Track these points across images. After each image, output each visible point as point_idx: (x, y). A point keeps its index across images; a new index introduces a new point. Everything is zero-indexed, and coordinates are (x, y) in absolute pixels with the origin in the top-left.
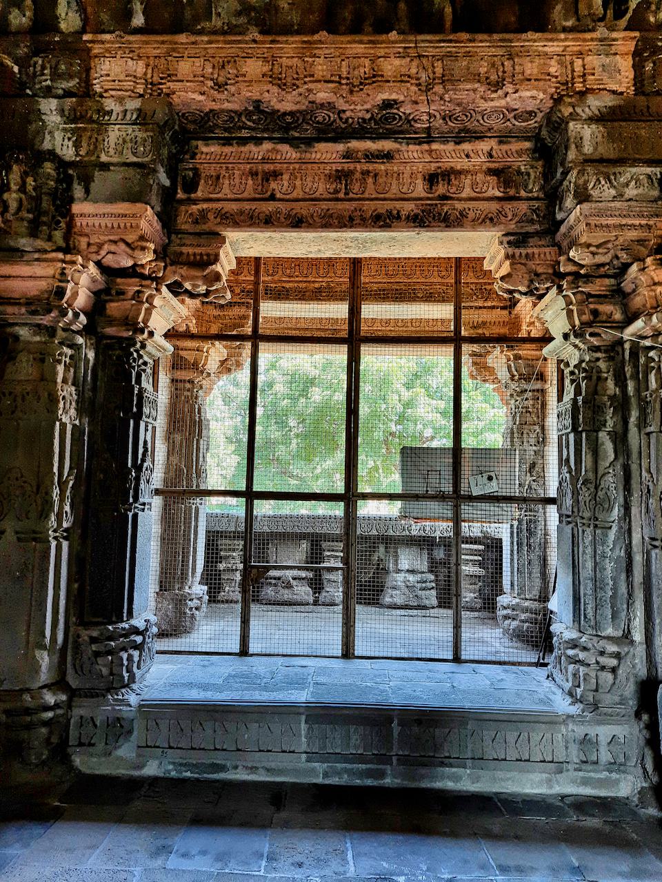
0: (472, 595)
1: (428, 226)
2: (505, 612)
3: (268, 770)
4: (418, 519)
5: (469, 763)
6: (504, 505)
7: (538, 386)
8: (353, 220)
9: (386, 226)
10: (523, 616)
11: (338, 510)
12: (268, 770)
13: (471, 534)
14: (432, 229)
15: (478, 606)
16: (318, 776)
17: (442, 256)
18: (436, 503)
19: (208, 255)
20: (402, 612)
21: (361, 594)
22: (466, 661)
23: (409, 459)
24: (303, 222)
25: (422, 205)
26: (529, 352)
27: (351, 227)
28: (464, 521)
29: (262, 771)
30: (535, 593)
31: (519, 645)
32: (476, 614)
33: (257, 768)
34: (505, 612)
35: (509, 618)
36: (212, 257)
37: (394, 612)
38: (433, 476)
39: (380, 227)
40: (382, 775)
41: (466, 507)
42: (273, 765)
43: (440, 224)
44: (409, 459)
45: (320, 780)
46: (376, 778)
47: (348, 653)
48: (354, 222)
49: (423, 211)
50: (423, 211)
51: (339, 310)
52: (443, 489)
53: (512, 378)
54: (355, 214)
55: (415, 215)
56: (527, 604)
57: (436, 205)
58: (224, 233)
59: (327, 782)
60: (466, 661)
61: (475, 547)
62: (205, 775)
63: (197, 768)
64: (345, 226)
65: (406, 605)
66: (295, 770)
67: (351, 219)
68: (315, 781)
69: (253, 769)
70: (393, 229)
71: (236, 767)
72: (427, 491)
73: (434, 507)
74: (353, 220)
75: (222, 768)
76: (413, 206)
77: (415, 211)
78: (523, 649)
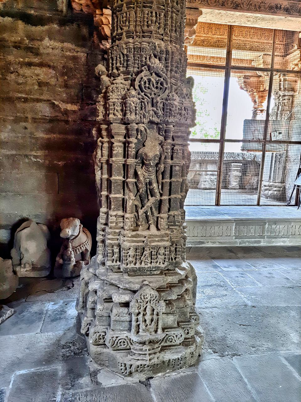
0: (235, 183)
1: (292, 14)
2: (266, 188)
3: (220, 243)
4: (248, 150)
5: (291, 236)
6: (282, 145)
7: (291, 93)
8: (261, 8)
9: (274, 13)
10: (275, 189)
11: (215, 148)
12: (220, 243)
13: (239, 159)
14: (293, 16)
15: (238, 188)
16: (238, 244)
17: (284, 29)
18: (257, 144)
19: (193, 20)
20: (209, 191)
21: (224, 181)
22: (262, 205)
23: (247, 125)
24: (238, 7)
25: (291, 3)
26: (291, 78)
27: (260, 11)
28: (267, 151)
29: (217, 243)
30: (280, 180)
31: (272, 200)
32: (237, 191)
33: (216, 242)
34: (266, 188)
35: (267, 190)
36: (194, 21)
37: (205, 191)
38: (256, 132)
39: (272, 13)
40: (260, 242)
41: (268, 146)
42: (221, 241)
43: (297, 14)
44: (247, 125)
45: (238, 245)
46: (258, 243)
47: (218, 204)
48: (261, 9)
49: (291, 6)
50: (291, 6)
51: (223, 53)
52: (259, 138)
53: (280, 89)
54: (261, 5)
55: (287, 8)
56: (276, 184)
57: (296, 3)
58: (201, 9)
59: (241, 246)
60: (262, 205)
61: (238, 164)
62: (197, 245)
63: (194, 243)
64: (257, 11)
65: (210, 188)
66: (230, 242)
67: (260, 7)
68: (236, 245)
69: (214, 243)
70: (276, 14)
71: (208, 242)
72: (253, 139)
73: (255, 145)
74: (261, 8)
75: (203, 243)
76: (287, 3)
77: (288, 6)
78: (273, 201)
